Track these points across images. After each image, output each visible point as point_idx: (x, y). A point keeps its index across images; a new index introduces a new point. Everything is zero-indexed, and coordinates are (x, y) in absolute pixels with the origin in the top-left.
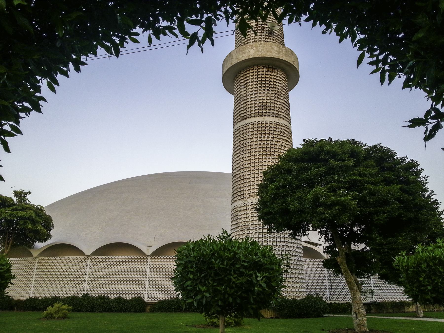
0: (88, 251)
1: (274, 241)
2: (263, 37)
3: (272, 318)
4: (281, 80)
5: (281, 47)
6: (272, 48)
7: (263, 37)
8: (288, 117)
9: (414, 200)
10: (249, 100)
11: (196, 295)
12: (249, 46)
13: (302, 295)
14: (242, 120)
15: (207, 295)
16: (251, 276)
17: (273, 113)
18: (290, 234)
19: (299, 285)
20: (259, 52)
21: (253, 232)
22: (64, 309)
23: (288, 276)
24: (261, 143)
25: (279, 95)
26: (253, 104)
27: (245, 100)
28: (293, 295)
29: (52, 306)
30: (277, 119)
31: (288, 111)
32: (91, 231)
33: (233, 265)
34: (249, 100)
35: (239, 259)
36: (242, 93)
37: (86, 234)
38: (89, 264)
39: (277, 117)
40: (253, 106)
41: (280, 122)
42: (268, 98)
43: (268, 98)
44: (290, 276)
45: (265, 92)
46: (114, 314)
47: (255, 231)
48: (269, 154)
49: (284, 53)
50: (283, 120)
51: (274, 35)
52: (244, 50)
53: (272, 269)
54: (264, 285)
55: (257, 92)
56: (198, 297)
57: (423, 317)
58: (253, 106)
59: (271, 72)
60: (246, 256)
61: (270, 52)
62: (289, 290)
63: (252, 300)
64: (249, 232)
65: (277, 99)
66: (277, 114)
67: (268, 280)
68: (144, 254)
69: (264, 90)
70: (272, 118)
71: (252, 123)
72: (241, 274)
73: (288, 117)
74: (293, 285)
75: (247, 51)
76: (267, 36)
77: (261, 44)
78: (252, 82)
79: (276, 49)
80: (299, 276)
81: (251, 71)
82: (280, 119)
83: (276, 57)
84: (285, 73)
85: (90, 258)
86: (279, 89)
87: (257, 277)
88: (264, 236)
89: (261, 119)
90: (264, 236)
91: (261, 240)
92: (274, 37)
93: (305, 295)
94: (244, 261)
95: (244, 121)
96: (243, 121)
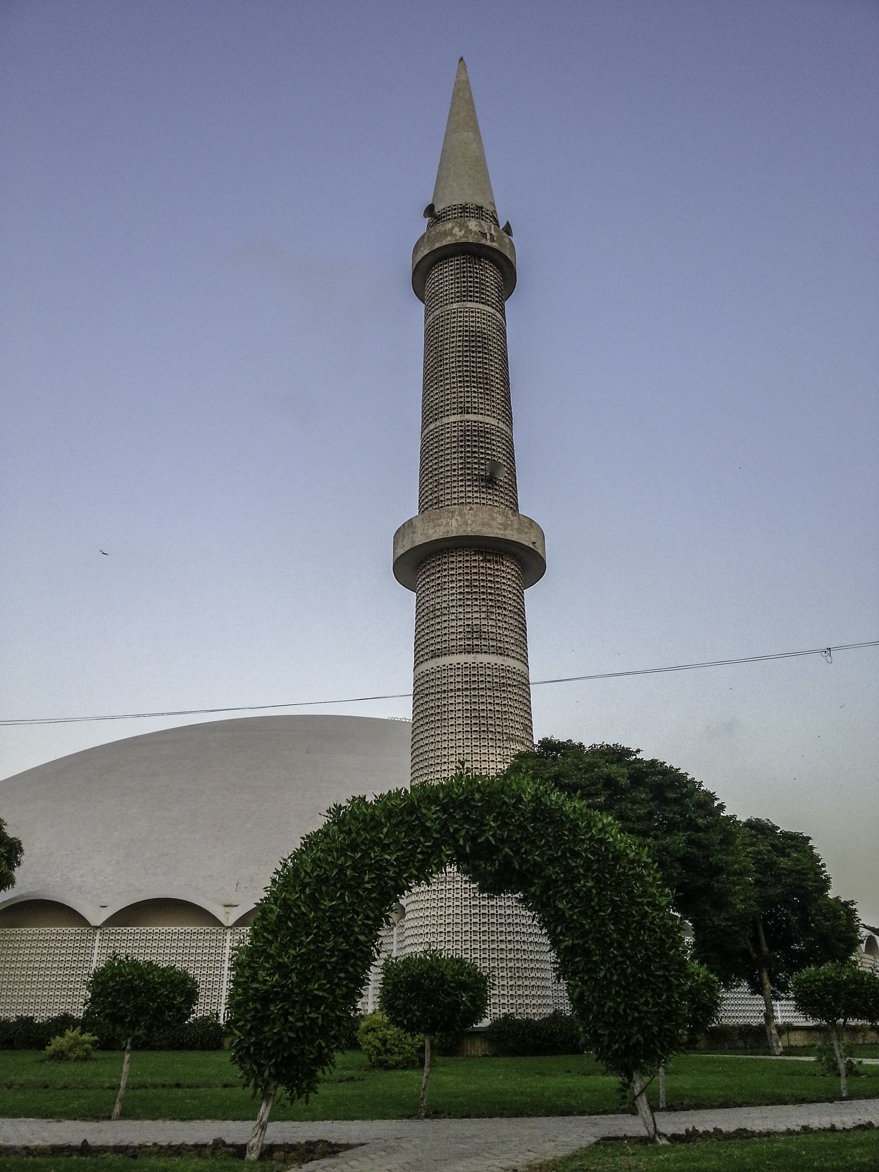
0: (97, 917)
1: (492, 906)
2: (476, 489)
3: (486, 1056)
4: (509, 577)
5: (510, 515)
6: (493, 519)
7: (476, 489)
8: (522, 652)
9: (707, 857)
10: (446, 618)
11: (406, 1014)
12: (448, 511)
13: (545, 1011)
14: (432, 657)
15: (418, 1014)
16: (457, 996)
17: (493, 646)
18: (520, 901)
19: (539, 993)
20: (467, 525)
21: (451, 887)
22: (84, 1042)
23: (517, 974)
24: (468, 707)
25: (505, 609)
26: (454, 626)
27: (438, 616)
28: (527, 1011)
29: (62, 1035)
30: (501, 658)
31: (522, 639)
32: (93, 869)
33: (442, 985)
34: (446, 618)
35: (447, 979)
36: (432, 602)
37: (82, 876)
38: (97, 944)
39: (501, 654)
40: (454, 630)
41: (506, 665)
42: (483, 615)
43: (483, 615)
44: (521, 974)
45: (478, 603)
46: (154, 1053)
47: (456, 886)
48: (484, 731)
49: (516, 526)
50: (512, 660)
51: (496, 484)
52: (437, 519)
53: (477, 988)
54: (468, 1004)
55: (461, 603)
56: (409, 1016)
57: (781, 1054)
58: (454, 630)
59: (489, 561)
60: (453, 976)
61: (490, 525)
62: (519, 1002)
63: (458, 1018)
64: (443, 887)
65: (500, 618)
66: (500, 647)
67: (473, 1000)
68: (218, 923)
69: (476, 599)
70: (491, 656)
71: (452, 667)
72: (449, 994)
73: (522, 652)
74: (526, 993)
75: (444, 521)
76: (483, 487)
77: (471, 509)
78: (452, 581)
79: (500, 519)
80: (538, 975)
81: (451, 559)
82: (506, 658)
83: (500, 536)
84: (517, 561)
85: (98, 932)
86: (504, 596)
87: (462, 997)
88: (472, 895)
89: (469, 658)
90: (472, 895)
91: (467, 903)
92: (496, 490)
93: (550, 1011)
94: (451, 982)
95: (437, 659)
96: (435, 660)
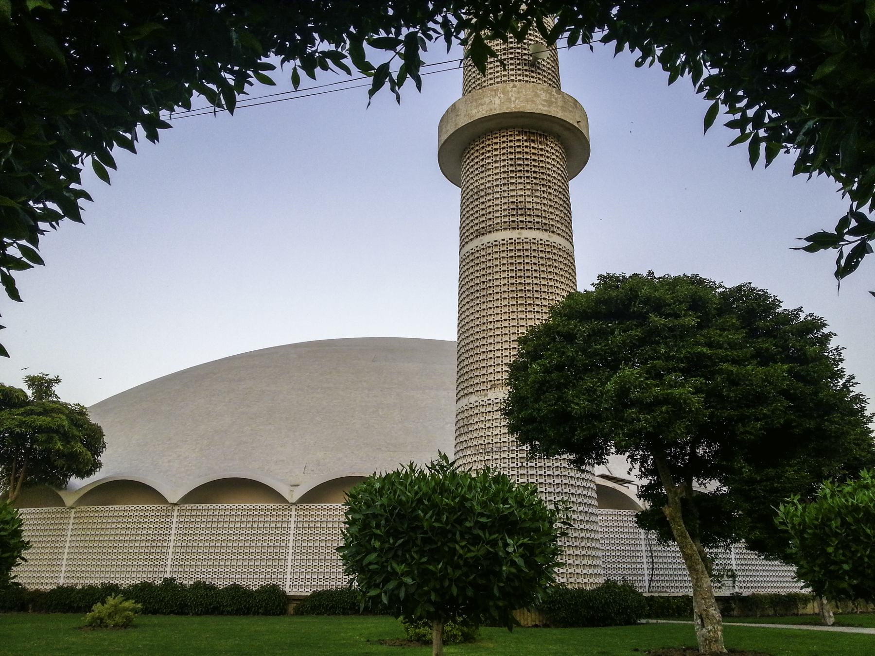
0: (173, 495)
1: (541, 475)
2: (519, 72)
3: (536, 626)
4: (553, 157)
5: (554, 93)
6: (537, 95)
7: (519, 72)
8: (567, 231)
9: (816, 393)
10: (490, 197)
11: (386, 581)
12: (492, 90)
13: (596, 581)
14: (477, 237)
15: (409, 581)
16: (494, 543)
17: (538, 223)
18: (571, 462)
19: (590, 562)
20: (510, 102)
21: (498, 457)
22: (126, 609)
23: (567, 544)
24: (514, 281)
25: (550, 187)
26: (498, 204)
27: (482, 197)
28: (578, 580)
29: (103, 602)
30: (547, 234)
31: (567, 218)
32: (179, 456)
33: (460, 521)
34: (490, 197)
35: (471, 510)
36: (476, 184)
37: (169, 461)
38: (175, 519)
39: (546, 230)
40: (498, 208)
41: (551, 240)
42: (528, 193)
43: (528, 193)
44: (571, 544)
45: (522, 181)
46: (225, 618)
47: (503, 456)
48: (530, 304)
49: (560, 104)
50: (557, 236)
51: (539, 68)
52: (481, 99)
53: (537, 530)
54: (520, 561)
55: (506, 181)
56: (391, 585)
57: (833, 625)
58: (498, 208)
59: (533, 141)
60: (484, 505)
61: (533, 101)
62: (570, 571)
63: (496, 592)
64: (490, 457)
65: (545, 195)
66: (545, 224)
67: (529, 552)
68: (284, 501)
69: (520, 177)
70: (537, 232)
71: (497, 243)
72: (476, 540)
73: (567, 231)
74: (577, 562)
75: (487, 100)
76: (526, 70)
77: (514, 86)
78: (496, 162)
79: (544, 96)
80: (589, 544)
81: (494, 141)
82: (551, 234)
83: (544, 112)
84: (562, 144)
85: (176, 508)
86: (549, 175)
87: (506, 545)
88: (520, 464)
89: (514, 234)
90: (520, 464)
91: (515, 472)
92: (539, 74)
93: (601, 580)
94: (481, 515)
95: (482, 238)
96: (479, 239)
